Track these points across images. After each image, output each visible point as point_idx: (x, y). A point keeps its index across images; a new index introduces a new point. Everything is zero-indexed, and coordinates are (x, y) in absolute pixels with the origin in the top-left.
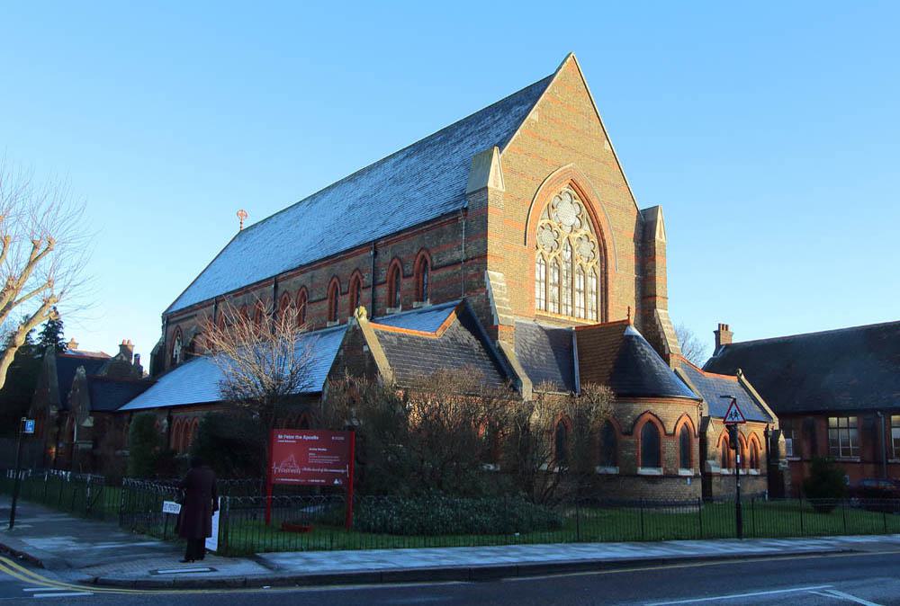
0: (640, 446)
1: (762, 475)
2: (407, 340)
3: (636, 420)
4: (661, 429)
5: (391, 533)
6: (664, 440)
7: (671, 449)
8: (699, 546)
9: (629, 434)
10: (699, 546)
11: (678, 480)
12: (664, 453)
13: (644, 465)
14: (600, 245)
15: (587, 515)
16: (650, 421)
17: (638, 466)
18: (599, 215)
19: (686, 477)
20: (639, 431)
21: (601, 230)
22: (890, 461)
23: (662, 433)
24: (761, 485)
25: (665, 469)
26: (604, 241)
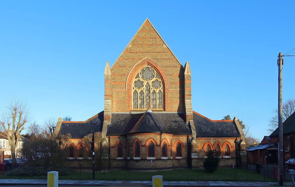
0: (134, 150)
1: (232, 158)
2: (73, 124)
3: (133, 141)
4: (140, 144)
5: (30, 176)
6: (141, 147)
7: (143, 150)
8: (80, 182)
9: (131, 146)
10: (80, 182)
11: (146, 161)
12: (141, 152)
13: (136, 157)
14: (162, 82)
15: (89, 172)
16: (137, 141)
17: (133, 156)
18: (160, 72)
19: (150, 160)
20: (134, 145)
21: (162, 76)
22: (285, 151)
23: (140, 145)
24: (233, 163)
25: (141, 157)
26: (163, 80)
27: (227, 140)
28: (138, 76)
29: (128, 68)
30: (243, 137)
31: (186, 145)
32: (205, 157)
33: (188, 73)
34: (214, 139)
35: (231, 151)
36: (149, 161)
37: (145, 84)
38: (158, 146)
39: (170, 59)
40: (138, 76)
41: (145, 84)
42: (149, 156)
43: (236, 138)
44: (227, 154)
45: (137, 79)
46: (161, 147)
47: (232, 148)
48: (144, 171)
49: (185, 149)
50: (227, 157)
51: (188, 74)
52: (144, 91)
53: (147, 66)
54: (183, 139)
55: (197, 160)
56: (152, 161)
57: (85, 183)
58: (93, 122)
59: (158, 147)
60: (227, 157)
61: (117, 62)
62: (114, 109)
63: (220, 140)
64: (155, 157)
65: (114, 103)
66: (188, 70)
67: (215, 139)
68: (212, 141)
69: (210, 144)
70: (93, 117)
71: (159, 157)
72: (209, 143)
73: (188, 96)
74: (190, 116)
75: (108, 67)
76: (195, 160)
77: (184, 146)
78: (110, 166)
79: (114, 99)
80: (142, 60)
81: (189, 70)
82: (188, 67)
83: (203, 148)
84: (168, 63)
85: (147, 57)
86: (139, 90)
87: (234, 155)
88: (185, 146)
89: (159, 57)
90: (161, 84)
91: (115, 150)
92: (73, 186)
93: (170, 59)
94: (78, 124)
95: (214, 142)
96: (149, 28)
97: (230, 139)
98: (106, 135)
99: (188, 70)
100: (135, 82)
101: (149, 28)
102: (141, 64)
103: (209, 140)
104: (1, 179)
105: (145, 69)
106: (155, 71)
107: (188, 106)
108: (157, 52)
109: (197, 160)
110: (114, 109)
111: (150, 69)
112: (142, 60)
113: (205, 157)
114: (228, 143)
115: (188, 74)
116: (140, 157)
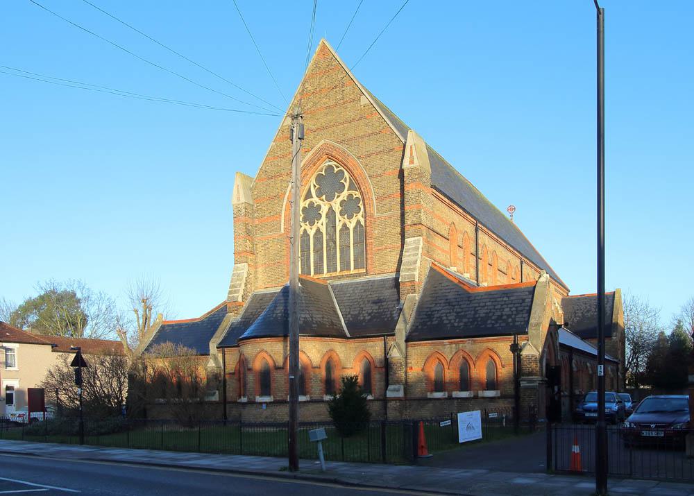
1: (503, 397)
11: (255, 405)
19: (261, 403)
25: (274, 397)
27: (491, 345)
28: (309, 195)
29: (285, 178)
30: (534, 332)
31: (381, 362)
32: (429, 393)
33: (412, 162)
34: (451, 343)
35: (500, 375)
36: (260, 407)
37: (324, 210)
38: (277, 368)
39: (376, 134)
40: (309, 195)
41: (324, 210)
42: (262, 395)
43: (513, 336)
44: (491, 385)
45: (308, 202)
46: (286, 371)
47: (503, 366)
48: (256, 430)
49: (380, 373)
50: (490, 394)
51: (412, 165)
52: (324, 230)
53: (327, 164)
54: (375, 348)
55: (398, 404)
56: (264, 405)
57: (188, 460)
58: (517, 324)
59: (279, 371)
60: (490, 394)
61: (264, 168)
62: (260, 283)
63: (468, 345)
64: (272, 397)
65: (260, 270)
66: (411, 154)
67: (455, 343)
68: (448, 349)
69: (441, 358)
70: (217, 308)
71: (316, 396)
72: (438, 356)
73: (414, 227)
74: (409, 284)
75: (238, 186)
76: (394, 402)
77: (376, 367)
78: (226, 419)
79: (260, 260)
80: (315, 149)
81: (414, 154)
82: (411, 147)
83: (423, 370)
84: (371, 145)
85: (322, 142)
86: (311, 229)
87: (510, 389)
88: (378, 365)
89: (351, 134)
90: (359, 205)
91: (234, 381)
92: (268, 472)
93: (376, 134)
94: (186, 324)
95: (453, 353)
96: (327, 65)
97: (498, 341)
98: (217, 348)
99: (411, 154)
100: (304, 209)
101: (327, 65)
102: (313, 162)
103: (440, 347)
104: (1, 439)
105: (323, 173)
106: (346, 173)
107: (409, 256)
108: (347, 122)
109: (398, 404)
110: (260, 283)
111: (336, 170)
112: (315, 149)
113: (429, 393)
114: (493, 354)
115: (412, 165)
116: (272, 397)
